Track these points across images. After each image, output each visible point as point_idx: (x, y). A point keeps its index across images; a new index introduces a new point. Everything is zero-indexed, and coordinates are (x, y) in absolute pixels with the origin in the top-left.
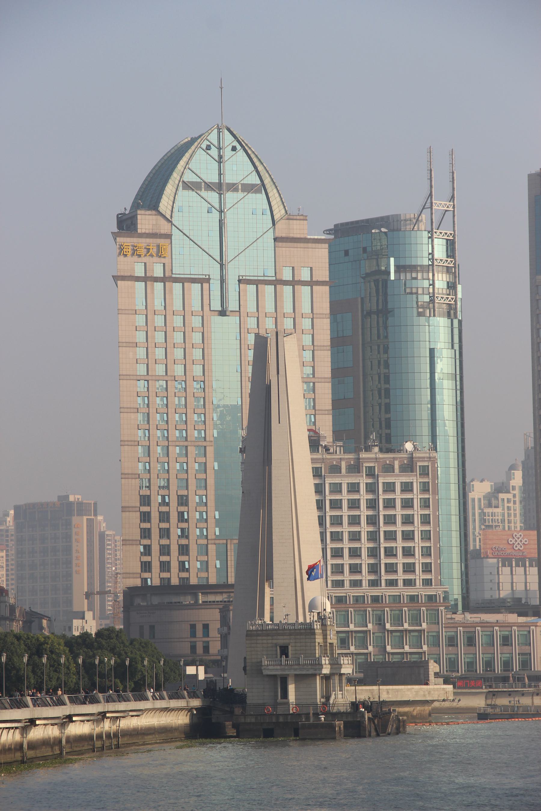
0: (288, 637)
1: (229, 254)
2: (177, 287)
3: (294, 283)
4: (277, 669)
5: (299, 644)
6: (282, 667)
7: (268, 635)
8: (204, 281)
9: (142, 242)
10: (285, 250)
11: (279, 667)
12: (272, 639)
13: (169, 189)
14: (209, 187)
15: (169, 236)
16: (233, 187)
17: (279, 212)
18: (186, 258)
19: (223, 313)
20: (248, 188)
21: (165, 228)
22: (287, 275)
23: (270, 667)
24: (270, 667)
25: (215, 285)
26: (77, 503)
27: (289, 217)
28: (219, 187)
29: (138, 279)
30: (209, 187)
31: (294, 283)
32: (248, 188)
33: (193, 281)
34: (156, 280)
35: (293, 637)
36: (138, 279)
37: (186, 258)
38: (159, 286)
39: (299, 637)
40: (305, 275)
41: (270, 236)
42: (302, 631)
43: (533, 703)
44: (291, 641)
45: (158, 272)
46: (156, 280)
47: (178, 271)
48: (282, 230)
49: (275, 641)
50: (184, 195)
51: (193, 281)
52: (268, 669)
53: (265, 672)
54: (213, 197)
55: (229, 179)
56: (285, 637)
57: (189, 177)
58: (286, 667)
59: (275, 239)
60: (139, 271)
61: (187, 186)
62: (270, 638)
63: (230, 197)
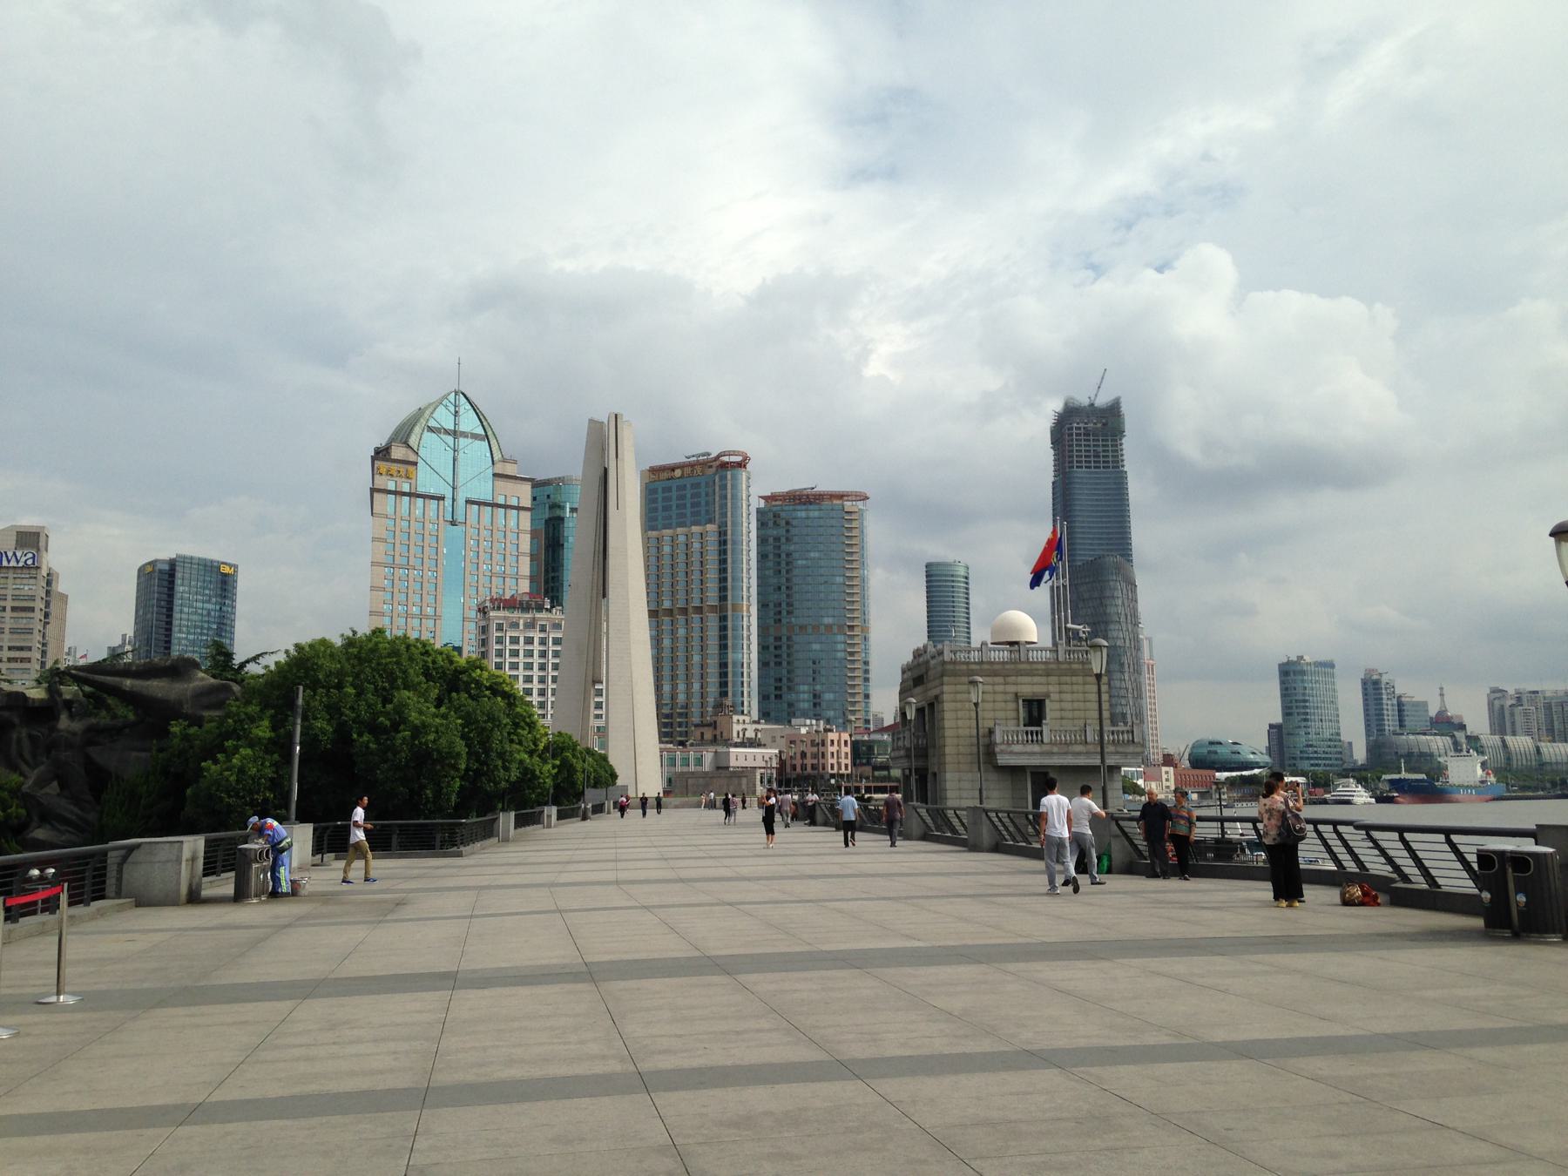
0: (1043, 680)
1: (461, 480)
2: (420, 501)
3: (506, 507)
4: (1034, 753)
5: (1068, 697)
6: (1045, 748)
7: (995, 674)
8: (441, 498)
9: (395, 467)
10: (500, 483)
11: (1036, 748)
12: (1006, 684)
13: (417, 430)
14: (447, 432)
15: (415, 464)
16: (464, 434)
17: (497, 456)
18: (426, 481)
19: (453, 523)
20: (475, 437)
21: (412, 458)
22: (501, 500)
23: (1017, 748)
24: (1017, 748)
25: (448, 502)
26: (234, 842)
27: (504, 461)
28: (455, 434)
29: (390, 492)
30: (447, 432)
31: (506, 507)
32: (475, 437)
33: (432, 498)
34: (404, 494)
35: (1053, 679)
36: (390, 492)
37: (426, 481)
38: (406, 499)
39: (1068, 679)
40: (514, 502)
41: (490, 472)
42: (1075, 666)
43: (1223, 833)
44: (1051, 688)
45: (406, 488)
46: (404, 494)
47: (421, 490)
48: (499, 469)
49: (1012, 689)
50: (427, 435)
51: (432, 498)
52: (1011, 753)
53: (1003, 760)
54: (450, 439)
55: (462, 428)
56: (1036, 679)
57: (432, 423)
58: (1055, 749)
59: (495, 475)
60: (391, 486)
61: (430, 429)
62: (1000, 679)
63: (462, 441)
